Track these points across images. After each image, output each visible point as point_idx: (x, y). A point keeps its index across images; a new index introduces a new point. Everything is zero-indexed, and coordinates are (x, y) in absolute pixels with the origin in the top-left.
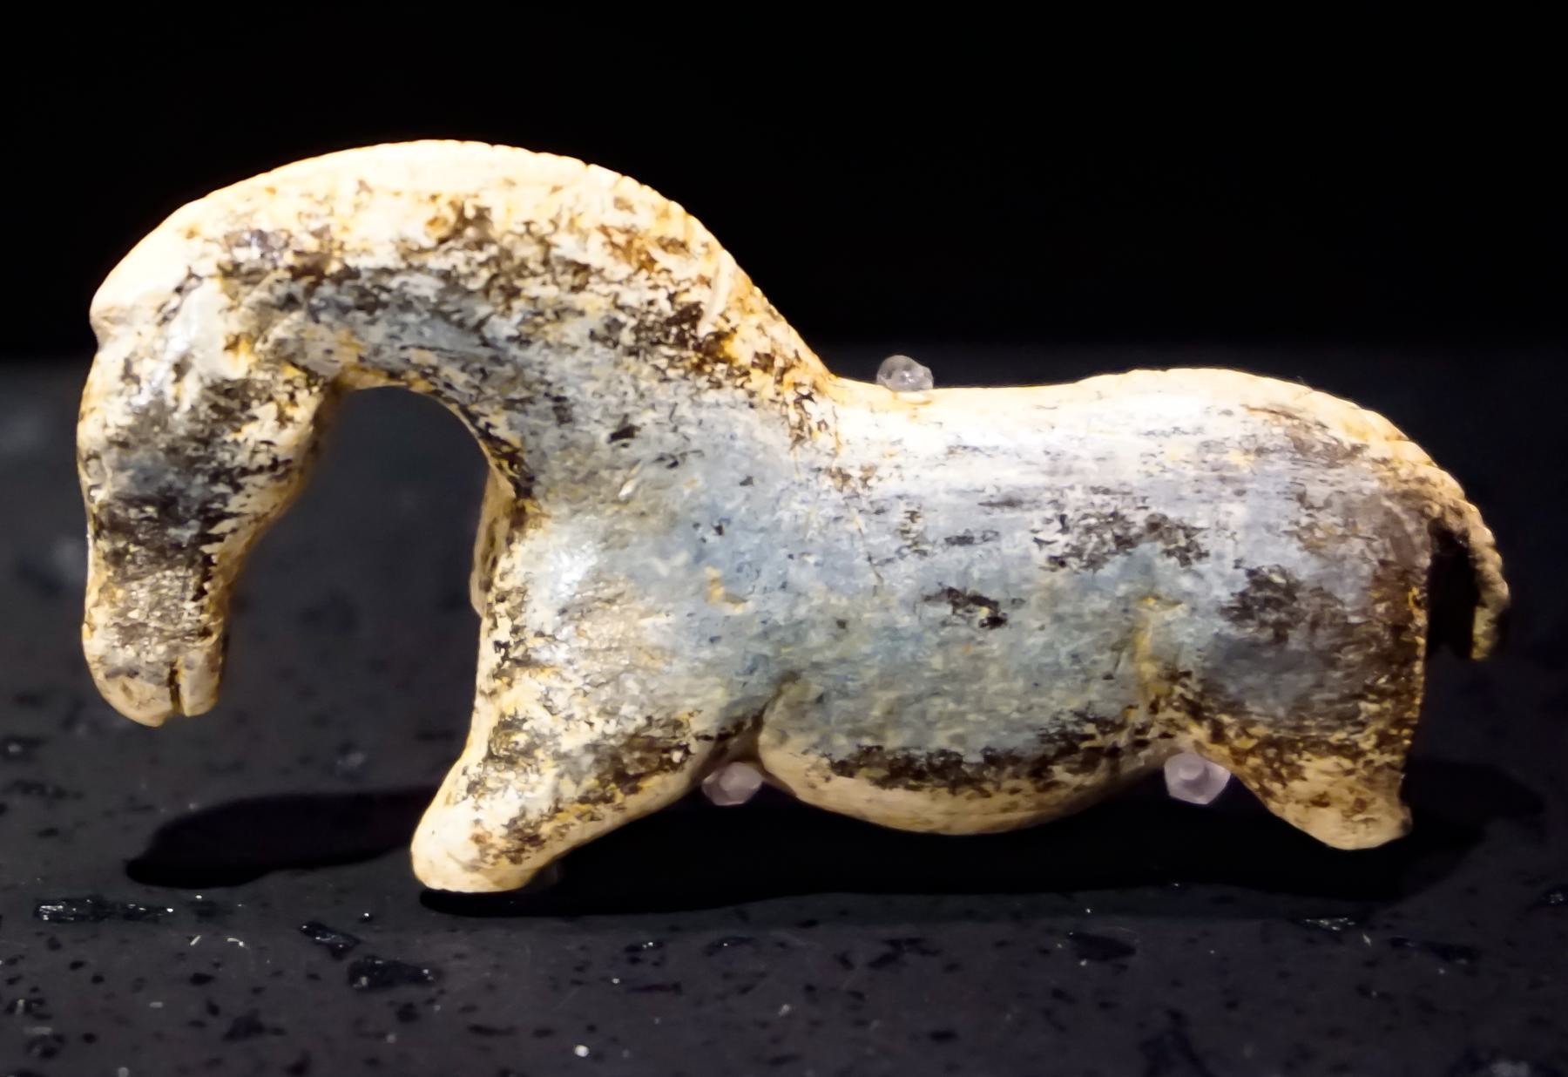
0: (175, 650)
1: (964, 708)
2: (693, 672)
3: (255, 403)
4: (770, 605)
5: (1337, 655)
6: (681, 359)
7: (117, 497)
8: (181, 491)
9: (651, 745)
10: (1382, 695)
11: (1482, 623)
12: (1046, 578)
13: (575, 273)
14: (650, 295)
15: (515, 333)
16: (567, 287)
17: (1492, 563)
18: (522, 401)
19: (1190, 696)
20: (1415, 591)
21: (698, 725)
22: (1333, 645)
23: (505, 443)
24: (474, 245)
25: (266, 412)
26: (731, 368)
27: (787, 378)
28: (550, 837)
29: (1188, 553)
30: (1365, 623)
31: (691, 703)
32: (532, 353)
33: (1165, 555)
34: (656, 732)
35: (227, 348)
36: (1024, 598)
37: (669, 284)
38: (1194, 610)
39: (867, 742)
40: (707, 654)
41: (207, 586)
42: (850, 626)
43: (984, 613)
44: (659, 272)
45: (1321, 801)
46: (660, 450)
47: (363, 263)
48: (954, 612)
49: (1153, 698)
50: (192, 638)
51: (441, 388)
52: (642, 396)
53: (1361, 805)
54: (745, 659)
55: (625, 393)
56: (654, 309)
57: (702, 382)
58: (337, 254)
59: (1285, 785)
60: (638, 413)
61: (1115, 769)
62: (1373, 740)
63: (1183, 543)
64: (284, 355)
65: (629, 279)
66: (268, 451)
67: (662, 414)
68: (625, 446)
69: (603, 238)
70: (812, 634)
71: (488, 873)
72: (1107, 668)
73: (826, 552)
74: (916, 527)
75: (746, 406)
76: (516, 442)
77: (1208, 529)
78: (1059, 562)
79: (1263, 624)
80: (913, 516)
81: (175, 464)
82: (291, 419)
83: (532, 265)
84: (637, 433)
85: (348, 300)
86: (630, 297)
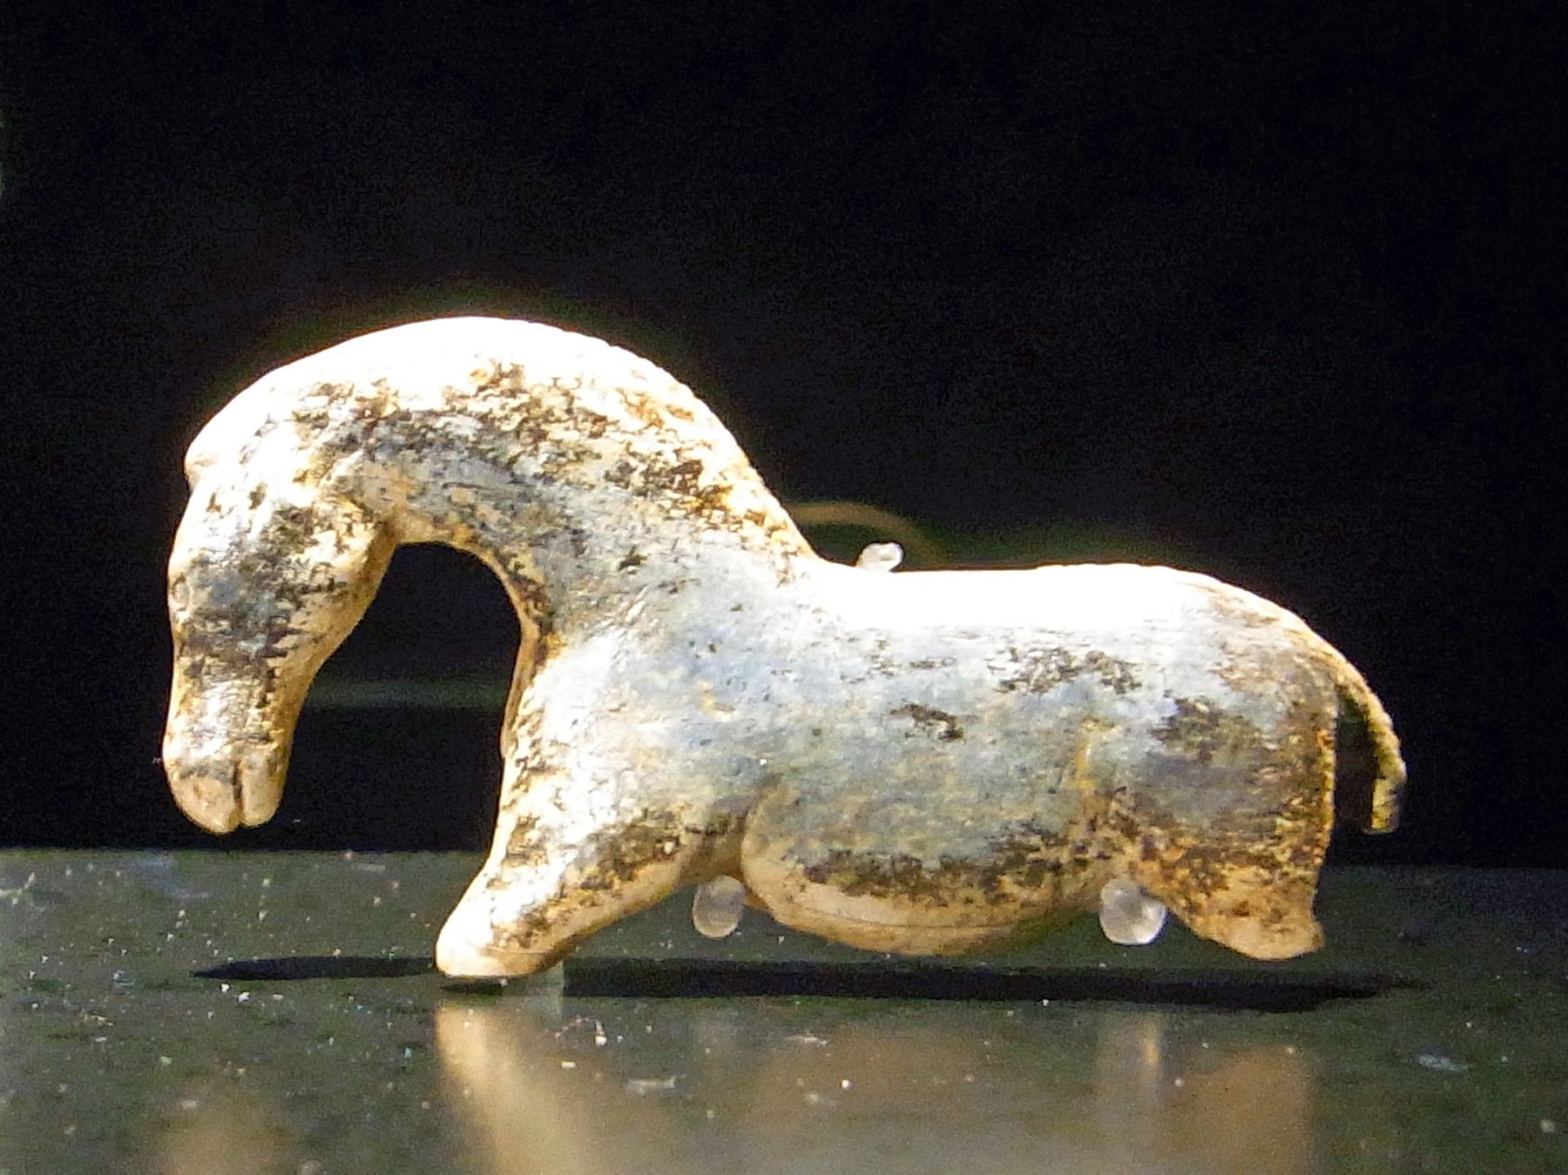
0: (240, 750)
1: (924, 814)
2: (685, 769)
3: (317, 529)
4: (754, 715)
5: (1255, 775)
6: (683, 503)
7: (197, 613)
8: (251, 608)
9: (646, 834)
10: (1296, 815)
11: (1381, 797)
12: (999, 699)
13: (594, 422)
14: (659, 447)
15: (541, 471)
16: (587, 433)
17: (1390, 742)
18: (546, 536)
19: (1124, 812)
20: (1324, 733)
21: (688, 819)
22: (1250, 766)
23: (531, 582)
24: (509, 393)
25: (326, 539)
26: (726, 515)
27: (775, 534)
28: (555, 921)
29: (1124, 685)
30: (1281, 750)
31: (682, 798)
32: (555, 489)
33: (1103, 685)
34: (650, 824)
35: (296, 480)
36: (978, 714)
37: (674, 440)
38: (1129, 730)
39: (838, 846)
40: (698, 754)
41: (270, 696)
42: (824, 735)
43: (942, 727)
44: (667, 430)
45: (1241, 911)
46: (663, 578)
47: (415, 406)
48: (916, 726)
49: (1091, 815)
50: (253, 741)
51: (478, 531)
52: (648, 531)
53: (1278, 915)
54: (730, 760)
55: (634, 528)
56: (661, 458)
57: (701, 522)
58: (392, 399)
59: (1209, 895)
60: (644, 545)
61: (1057, 887)
62: (1288, 854)
63: (1118, 674)
64: (348, 491)
65: (640, 432)
66: (327, 572)
67: (665, 547)
68: (633, 573)
69: (621, 397)
70: (791, 741)
71: (501, 957)
72: (1050, 782)
73: (804, 670)
74: (885, 653)
75: (739, 547)
76: (540, 580)
77: (1141, 664)
78: (1010, 686)
79: (1190, 745)
80: (882, 645)
81: (249, 580)
82: (347, 547)
83: (558, 413)
84: (642, 562)
85: (400, 439)
86: (640, 446)
